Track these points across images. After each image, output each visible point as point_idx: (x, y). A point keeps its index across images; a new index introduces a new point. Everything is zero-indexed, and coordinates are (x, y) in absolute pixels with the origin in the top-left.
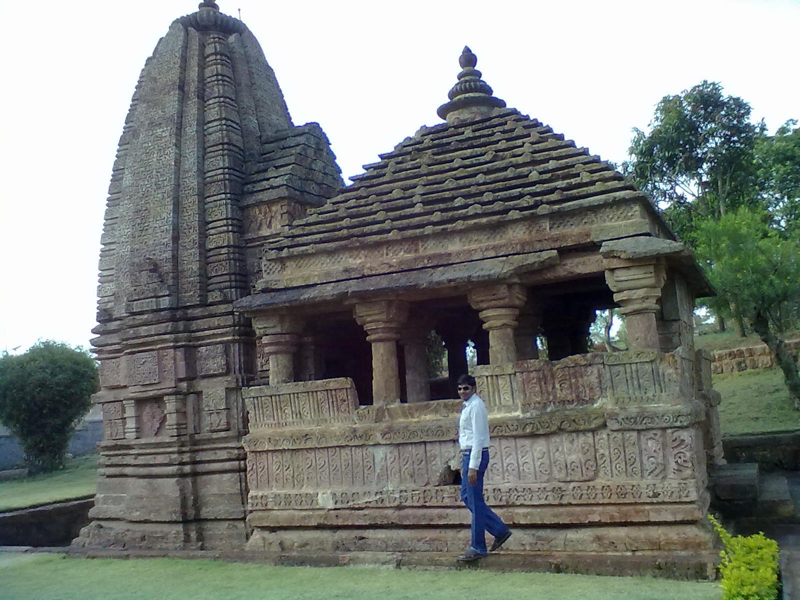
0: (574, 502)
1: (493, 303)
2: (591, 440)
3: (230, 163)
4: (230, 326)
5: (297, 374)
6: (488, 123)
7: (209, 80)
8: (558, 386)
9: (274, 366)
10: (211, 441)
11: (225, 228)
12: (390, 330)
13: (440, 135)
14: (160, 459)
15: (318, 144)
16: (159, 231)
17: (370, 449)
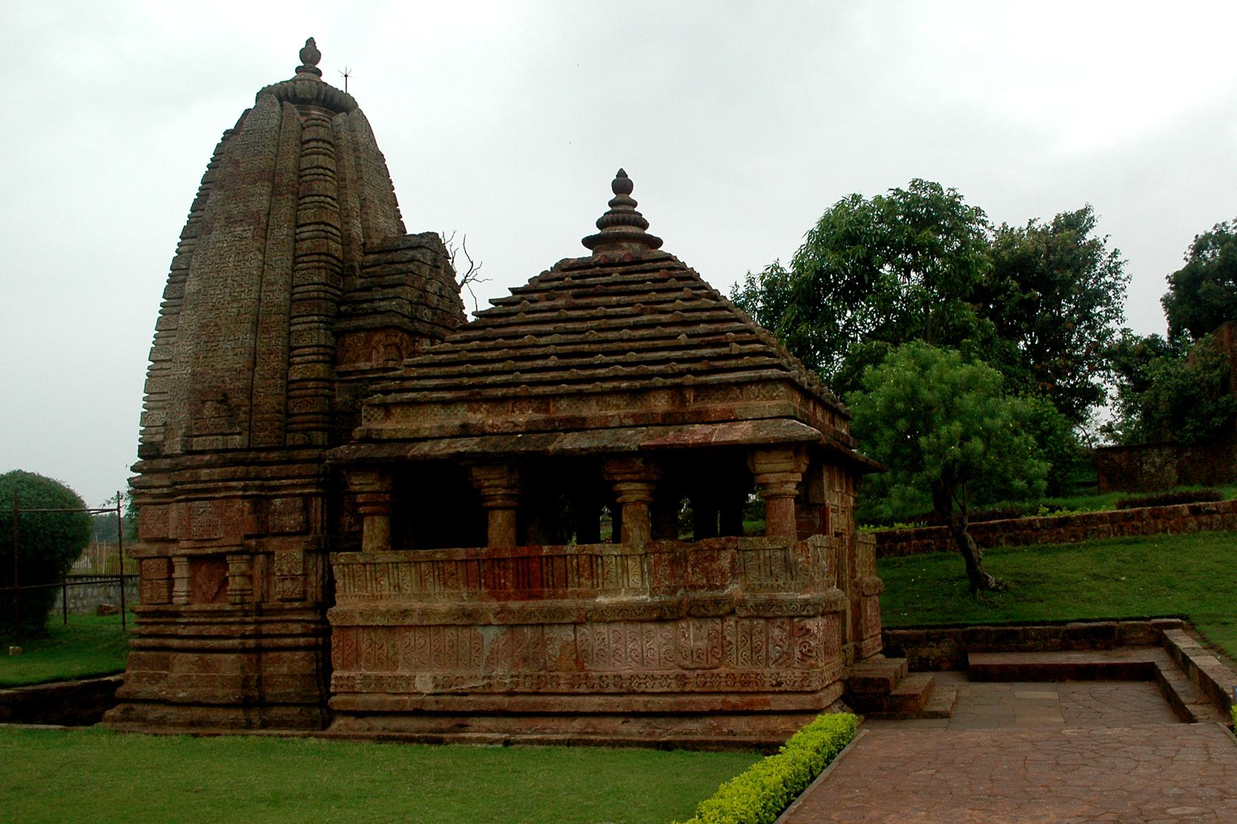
0: (697, 690)
1: (628, 476)
2: (719, 627)
4: (313, 476)
5: (396, 541)
8: (689, 570)
9: (374, 530)
10: (281, 611)
11: (315, 357)
12: (509, 496)
14: (215, 630)
15: (435, 260)
17: (480, 630)
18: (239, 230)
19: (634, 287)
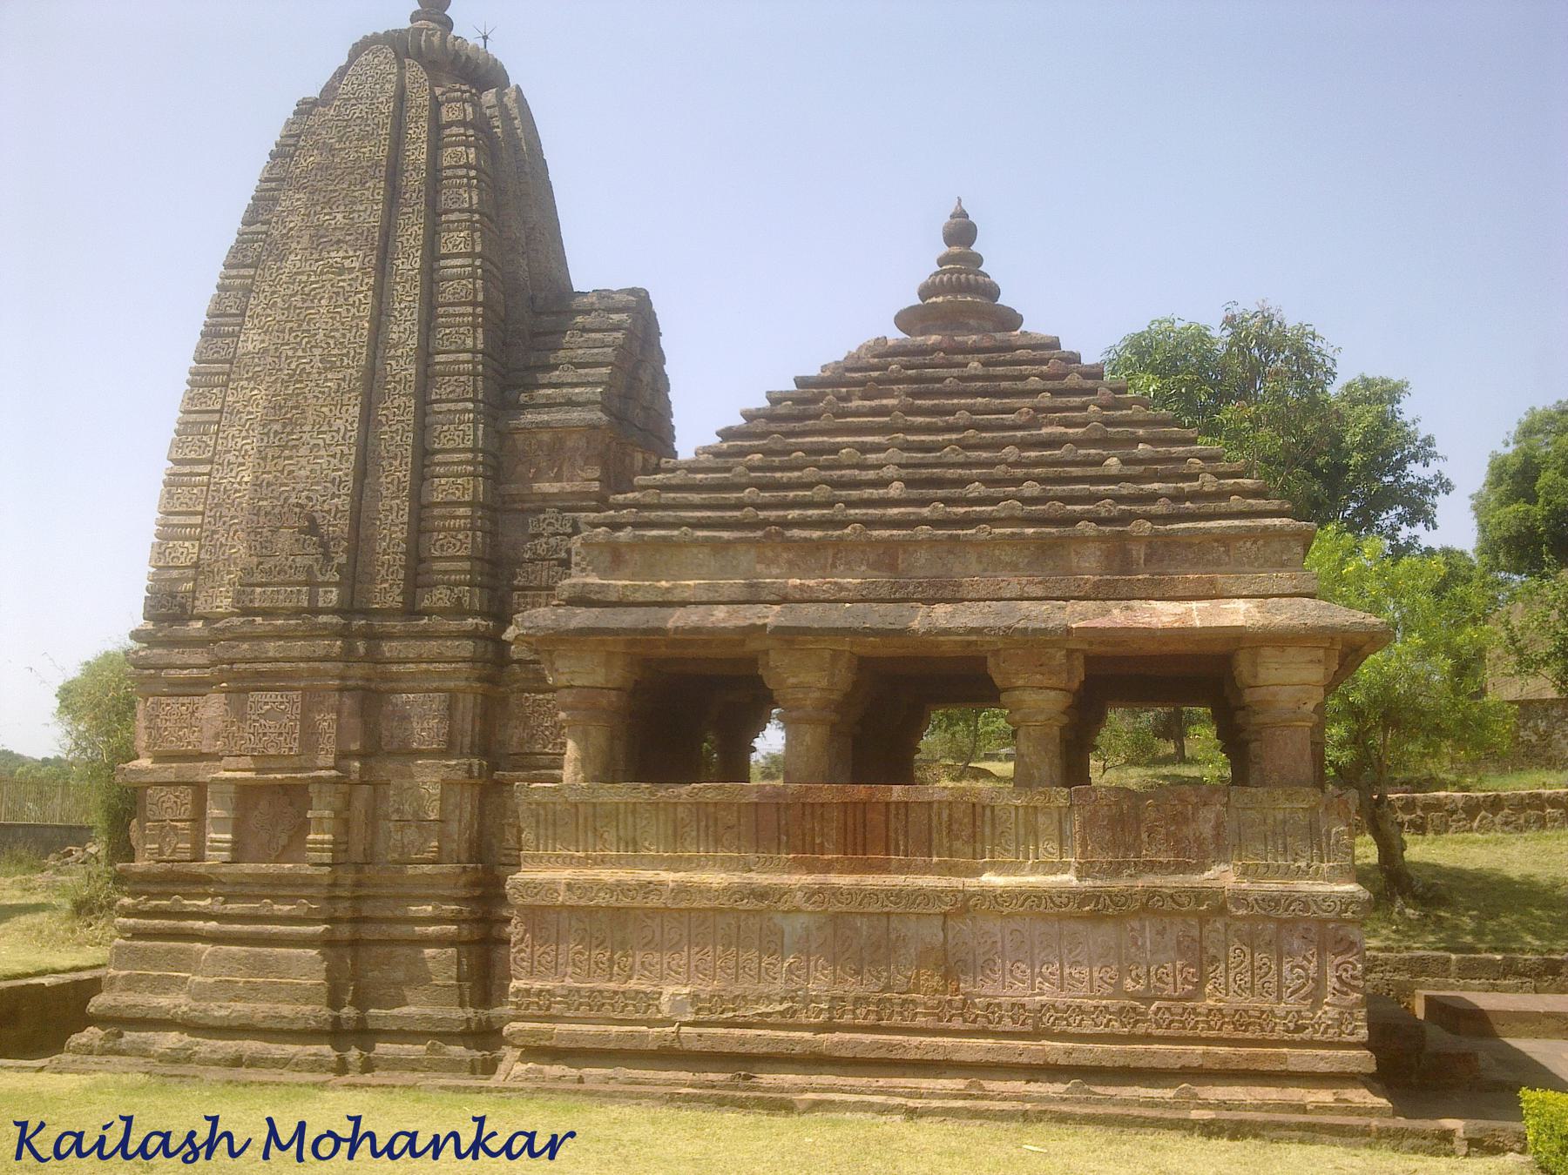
2: (1195, 933)
7: (449, 173)
13: (919, 360)
16: (323, 452)
18: (336, 256)
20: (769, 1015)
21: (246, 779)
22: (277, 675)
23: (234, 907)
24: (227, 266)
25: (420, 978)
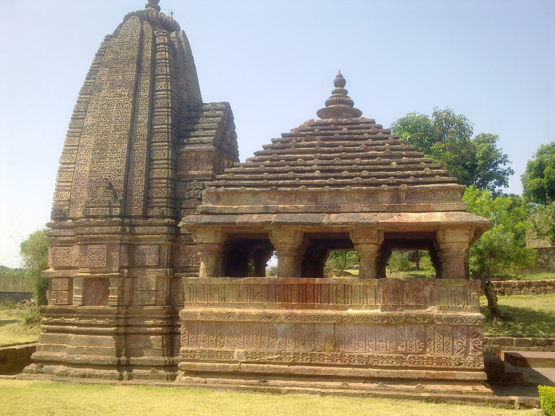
2: (423, 330)
3: (172, 121)
6: (357, 126)
7: (159, 61)
8: (405, 296)
16: (114, 160)
18: (119, 91)
19: (356, 136)
20: (272, 359)
21: (87, 276)
22: (98, 239)
23: (83, 321)
24: (80, 94)
25: (149, 347)
